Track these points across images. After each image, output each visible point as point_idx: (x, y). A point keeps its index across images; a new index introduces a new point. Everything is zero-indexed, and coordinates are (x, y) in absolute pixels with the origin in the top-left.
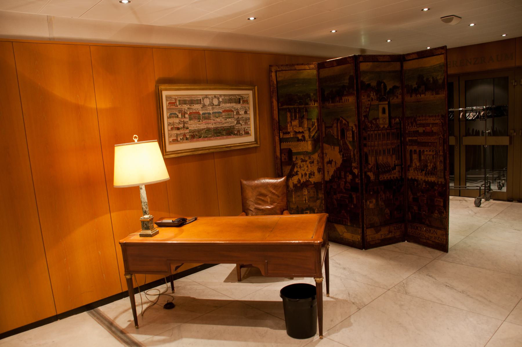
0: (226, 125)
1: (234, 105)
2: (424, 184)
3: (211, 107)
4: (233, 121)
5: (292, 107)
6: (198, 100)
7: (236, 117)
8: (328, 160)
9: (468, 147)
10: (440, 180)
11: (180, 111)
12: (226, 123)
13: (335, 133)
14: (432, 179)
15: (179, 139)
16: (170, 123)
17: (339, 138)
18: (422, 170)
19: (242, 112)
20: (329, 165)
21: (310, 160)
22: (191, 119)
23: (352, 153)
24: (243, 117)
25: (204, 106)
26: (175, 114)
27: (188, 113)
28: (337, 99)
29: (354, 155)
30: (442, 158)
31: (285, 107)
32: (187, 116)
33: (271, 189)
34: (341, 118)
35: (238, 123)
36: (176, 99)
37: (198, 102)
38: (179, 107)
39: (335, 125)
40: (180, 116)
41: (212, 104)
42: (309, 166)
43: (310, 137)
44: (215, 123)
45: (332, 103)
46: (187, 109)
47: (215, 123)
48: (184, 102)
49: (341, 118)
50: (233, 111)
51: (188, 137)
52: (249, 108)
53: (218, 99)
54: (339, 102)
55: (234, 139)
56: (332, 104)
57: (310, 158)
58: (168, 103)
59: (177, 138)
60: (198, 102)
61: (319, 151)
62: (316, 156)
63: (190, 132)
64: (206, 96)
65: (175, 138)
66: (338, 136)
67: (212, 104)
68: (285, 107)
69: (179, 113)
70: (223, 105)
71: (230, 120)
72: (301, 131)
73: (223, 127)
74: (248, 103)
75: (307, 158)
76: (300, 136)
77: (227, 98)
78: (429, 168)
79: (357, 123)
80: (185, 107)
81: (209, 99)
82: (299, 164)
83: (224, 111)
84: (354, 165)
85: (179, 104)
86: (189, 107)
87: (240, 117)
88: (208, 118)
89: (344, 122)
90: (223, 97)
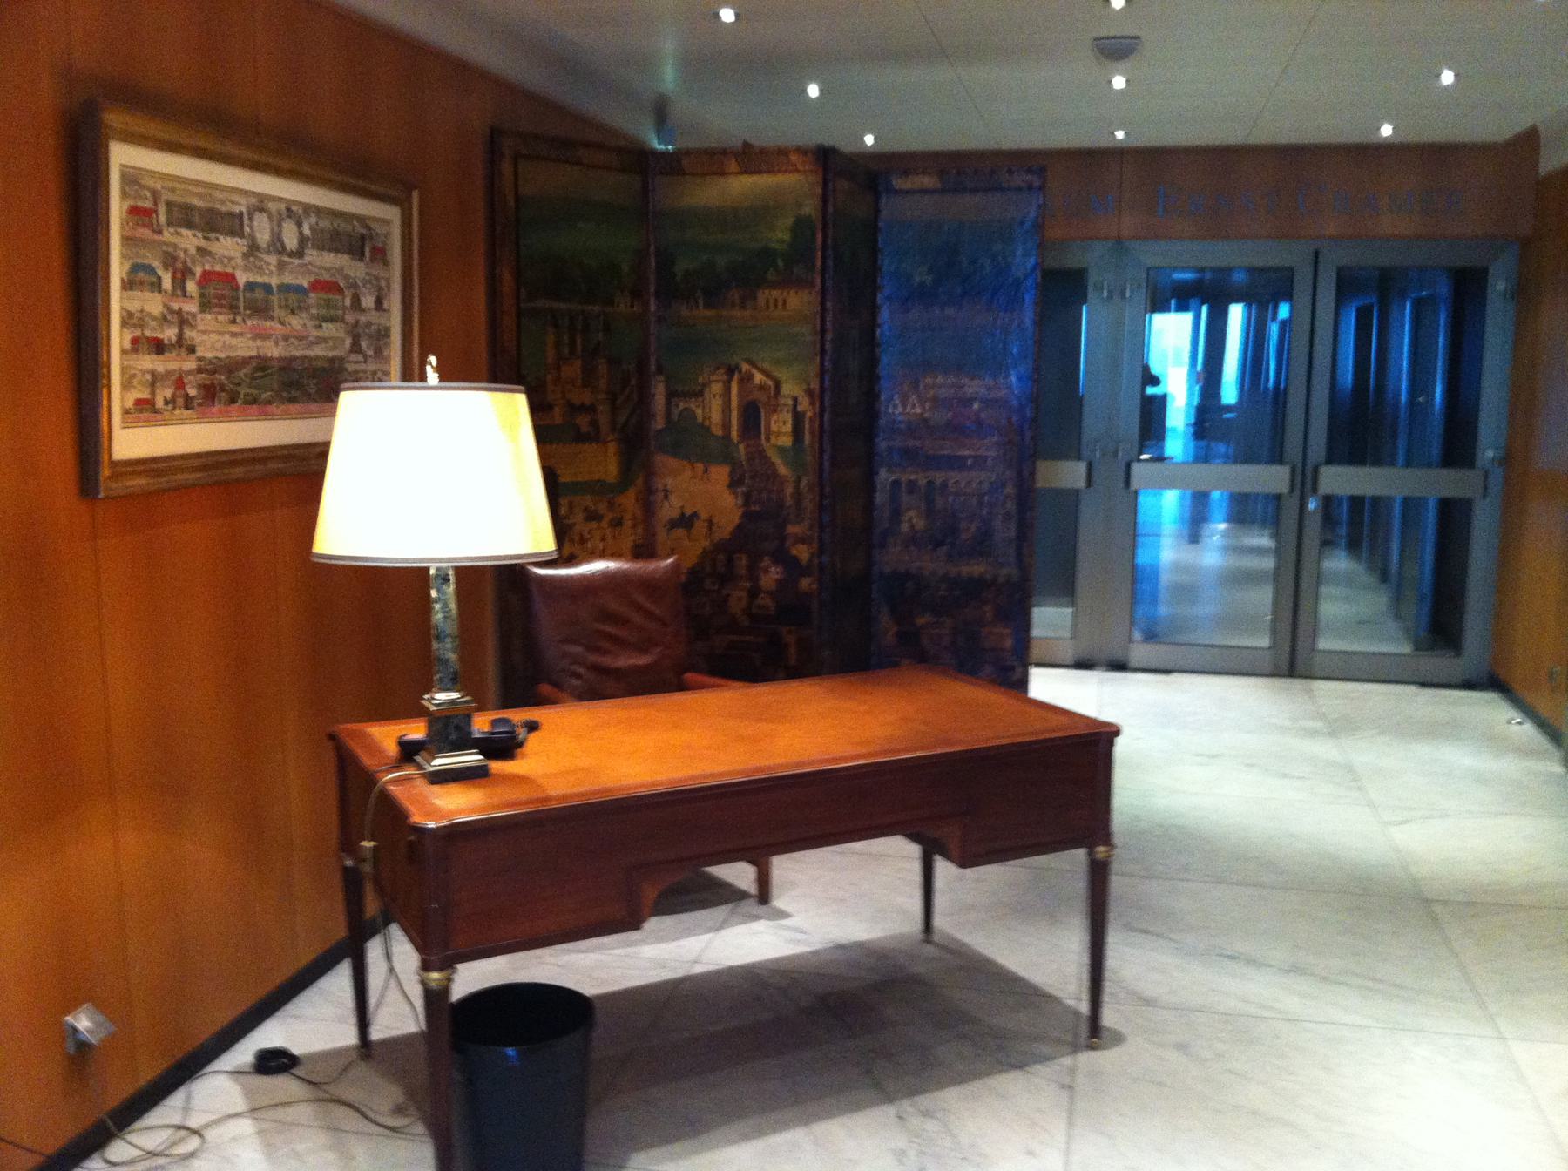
0: (318, 351)
1: (343, 260)
2: (943, 586)
3: (272, 259)
4: (341, 334)
5: (563, 306)
6: (231, 215)
7: (350, 318)
8: (675, 514)
9: (1277, 457)
10: (1005, 571)
11: (170, 260)
12: (321, 340)
13: (716, 417)
14: (977, 569)
15: (160, 403)
16: (130, 315)
17: (734, 434)
18: (938, 544)
19: (368, 301)
20: (680, 532)
21: (610, 516)
22: (205, 306)
23: (789, 490)
24: (369, 324)
25: (253, 248)
26: (150, 270)
27: (198, 271)
28: (735, 295)
29: (798, 496)
30: (1011, 506)
31: (541, 303)
32: (191, 286)
33: (641, 599)
34: (745, 367)
35: (356, 348)
36: (155, 195)
37: (232, 224)
38: (167, 235)
39: (717, 388)
40: (167, 283)
41: (277, 245)
42: (608, 532)
43: (613, 430)
44: (286, 338)
45: (708, 306)
46: (193, 251)
47: (286, 338)
48: (184, 216)
49: (745, 367)
50: (340, 290)
51: (192, 392)
52: (388, 280)
53: (299, 225)
54: (743, 307)
55: (188, 430)
56: (710, 313)
57: (611, 505)
58: (125, 208)
59: (153, 393)
60: (232, 224)
61: (640, 481)
62: (629, 501)
63: (200, 370)
64: (261, 204)
65: (146, 395)
66: (726, 426)
67: (277, 245)
68: (541, 303)
69: (166, 267)
70: (312, 255)
71: (329, 329)
72: (587, 402)
73: (309, 359)
74: (386, 263)
75: (602, 508)
76: (583, 421)
77: (325, 224)
78: (964, 536)
79: (815, 385)
80: (189, 240)
81: (270, 217)
82: (577, 529)
83: (317, 286)
84: (792, 529)
85: (170, 224)
86: (203, 243)
87: (363, 319)
88: (260, 310)
89: (758, 377)
90: (313, 220)
